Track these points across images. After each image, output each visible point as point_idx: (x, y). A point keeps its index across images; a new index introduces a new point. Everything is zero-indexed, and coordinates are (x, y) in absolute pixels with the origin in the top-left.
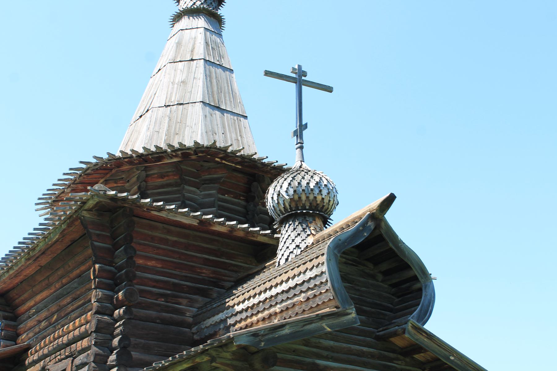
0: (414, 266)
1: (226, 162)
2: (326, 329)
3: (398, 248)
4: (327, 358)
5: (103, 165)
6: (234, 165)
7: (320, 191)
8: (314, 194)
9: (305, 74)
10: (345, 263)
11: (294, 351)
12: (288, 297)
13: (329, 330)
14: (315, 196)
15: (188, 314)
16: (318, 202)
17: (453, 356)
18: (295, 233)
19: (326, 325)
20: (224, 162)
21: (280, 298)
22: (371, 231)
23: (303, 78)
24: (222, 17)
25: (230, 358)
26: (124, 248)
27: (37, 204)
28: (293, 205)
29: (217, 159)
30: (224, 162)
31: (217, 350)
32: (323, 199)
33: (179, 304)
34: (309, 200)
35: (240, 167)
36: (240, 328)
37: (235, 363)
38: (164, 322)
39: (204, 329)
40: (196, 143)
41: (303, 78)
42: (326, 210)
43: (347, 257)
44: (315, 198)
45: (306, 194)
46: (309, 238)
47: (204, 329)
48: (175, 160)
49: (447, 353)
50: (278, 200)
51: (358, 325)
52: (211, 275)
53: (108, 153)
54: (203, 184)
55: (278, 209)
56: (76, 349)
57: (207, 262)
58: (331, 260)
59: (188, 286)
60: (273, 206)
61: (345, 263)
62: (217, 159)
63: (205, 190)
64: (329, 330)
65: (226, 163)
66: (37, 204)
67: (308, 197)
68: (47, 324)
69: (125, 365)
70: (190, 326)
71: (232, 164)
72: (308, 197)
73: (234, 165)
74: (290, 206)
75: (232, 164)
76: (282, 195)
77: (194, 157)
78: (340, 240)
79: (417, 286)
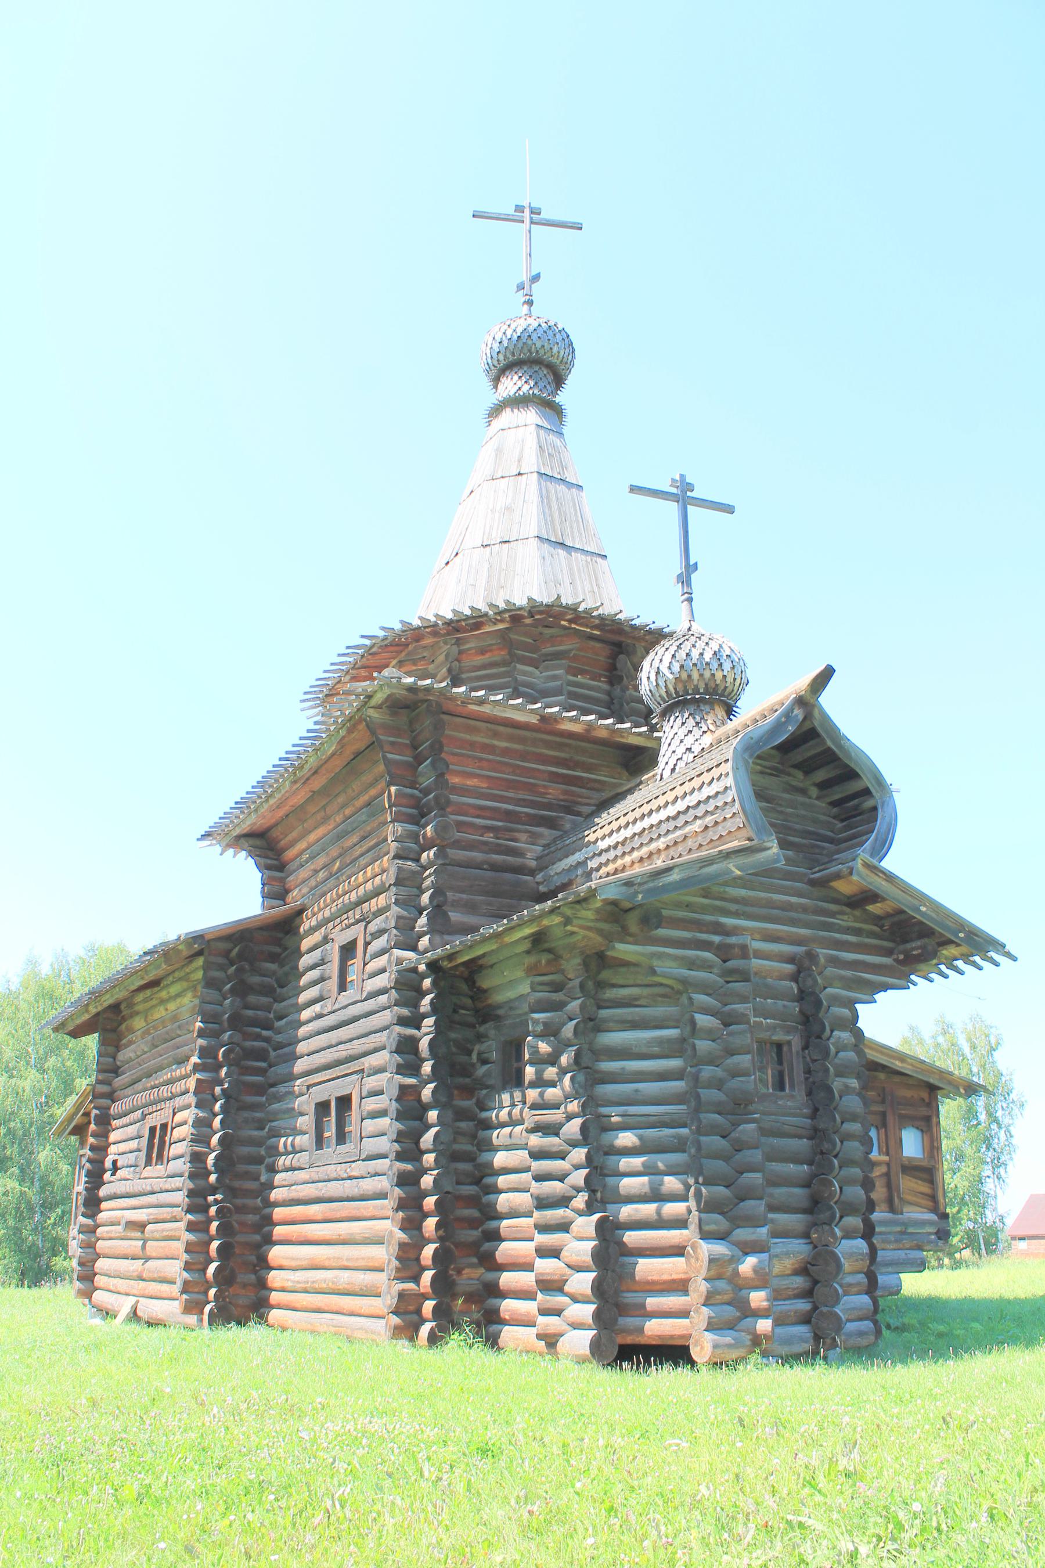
0: (864, 774)
2: (734, 872)
4: (736, 914)
6: (588, 630)
7: (721, 665)
9: (690, 487)
10: (762, 773)
11: (687, 906)
13: (739, 873)
15: (529, 855)
17: (925, 905)
18: (684, 730)
21: (664, 828)
23: (689, 494)
28: (680, 688)
29: (563, 623)
31: (572, 908)
35: (598, 633)
38: (495, 868)
40: (530, 599)
44: (713, 675)
48: (500, 626)
50: (656, 680)
52: (561, 797)
53: (402, 622)
54: (544, 661)
55: (658, 695)
60: (650, 691)
62: (563, 623)
63: (547, 669)
64: (739, 873)
65: (577, 627)
67: (701, 675)
70: (532, 872)
72: (701, 675)
73: (588, 630)
74: (675, 689)
78: (752, 738)
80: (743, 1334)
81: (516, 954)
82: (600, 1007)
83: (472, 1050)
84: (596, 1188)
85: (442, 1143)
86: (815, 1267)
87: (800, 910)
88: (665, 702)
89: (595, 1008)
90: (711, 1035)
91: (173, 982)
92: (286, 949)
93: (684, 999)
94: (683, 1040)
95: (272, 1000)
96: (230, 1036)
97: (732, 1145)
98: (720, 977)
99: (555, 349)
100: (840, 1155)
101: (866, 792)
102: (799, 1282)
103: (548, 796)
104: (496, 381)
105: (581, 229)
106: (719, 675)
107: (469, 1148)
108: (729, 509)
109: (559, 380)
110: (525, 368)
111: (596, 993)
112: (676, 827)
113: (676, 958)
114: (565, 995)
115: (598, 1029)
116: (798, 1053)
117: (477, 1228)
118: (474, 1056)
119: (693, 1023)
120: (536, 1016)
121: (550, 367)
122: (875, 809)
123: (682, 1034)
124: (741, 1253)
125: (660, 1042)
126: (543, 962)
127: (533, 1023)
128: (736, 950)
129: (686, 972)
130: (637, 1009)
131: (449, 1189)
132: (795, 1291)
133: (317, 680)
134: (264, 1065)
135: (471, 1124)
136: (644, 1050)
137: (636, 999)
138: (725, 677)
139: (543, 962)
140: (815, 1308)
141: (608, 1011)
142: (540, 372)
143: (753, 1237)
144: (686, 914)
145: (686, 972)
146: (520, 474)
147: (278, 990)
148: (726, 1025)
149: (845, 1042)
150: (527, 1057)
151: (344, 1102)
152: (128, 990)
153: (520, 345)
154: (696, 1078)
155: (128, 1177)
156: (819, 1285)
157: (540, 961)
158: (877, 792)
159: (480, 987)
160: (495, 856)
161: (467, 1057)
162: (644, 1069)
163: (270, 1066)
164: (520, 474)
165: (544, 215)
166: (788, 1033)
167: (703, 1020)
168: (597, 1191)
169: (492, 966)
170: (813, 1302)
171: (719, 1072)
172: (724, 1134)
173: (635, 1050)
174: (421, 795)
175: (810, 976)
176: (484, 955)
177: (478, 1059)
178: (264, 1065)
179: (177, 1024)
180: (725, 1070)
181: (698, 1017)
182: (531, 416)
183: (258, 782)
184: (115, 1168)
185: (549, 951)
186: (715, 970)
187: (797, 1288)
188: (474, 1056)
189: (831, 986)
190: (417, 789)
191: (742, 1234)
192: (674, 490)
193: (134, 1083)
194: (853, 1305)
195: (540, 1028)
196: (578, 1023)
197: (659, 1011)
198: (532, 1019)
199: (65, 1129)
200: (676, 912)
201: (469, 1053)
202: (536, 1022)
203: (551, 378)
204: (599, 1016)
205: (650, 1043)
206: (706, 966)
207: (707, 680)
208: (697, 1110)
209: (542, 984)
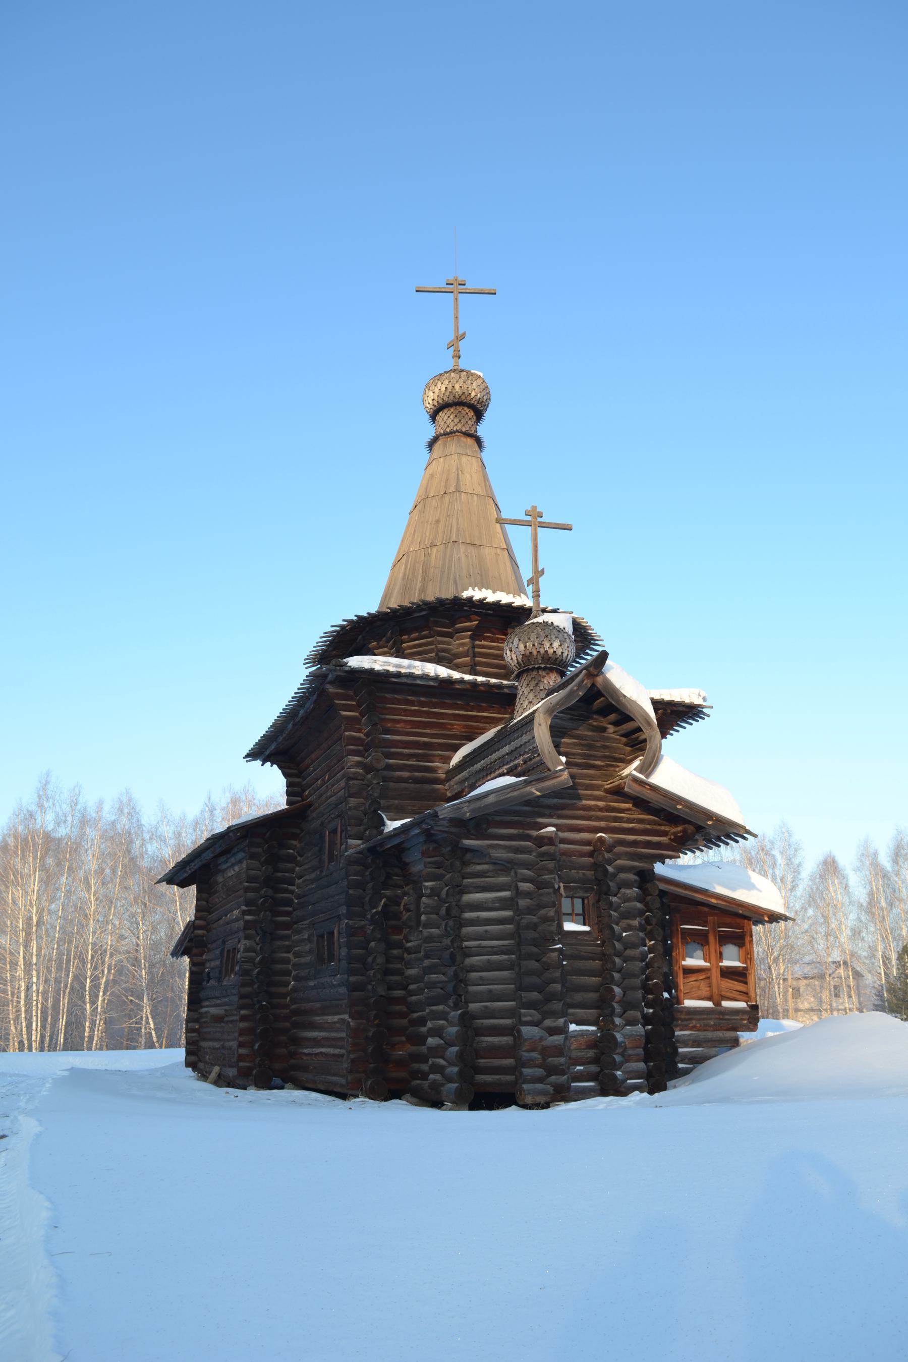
0: (637, 719)
3: (619, 701)
10: (571, 719)
11: (514, 813)
13: (538, 793)
15: (440, 771)
16: (550, 655)
17: (681, 804)
18: (528, 689)
22: (587, 689)
23: (539, 519)
25: (448, 825)
26: (368, 717)
27: (304, 664)
29: (465, 608)
31: (433, 820)
32: (555, 652)
37: (453, 830)
38: (416, 781)
39: (453, 786)
41: (539, 519)
42: (560, 662)
43: (573, 712)
44: (547, 651)
46: (542, 692)
47: (453, 786)
48: (424, 613)
49: (674, 803)
51: (511, 806)
52: (463, 730)
54: (456, 633)
58: (542, 724)
61: (571, 719)
62: (465, 608)
63: (459, 639)
64: (538, 793)
66: (304, 664)
67: (538, 652)
70: (442, 782)
74: (522, 661)
77: (441, 609)
78: (551, 704)
79: (643, 737)
80: (549, 1086)
82: (464, 878)
83: (401, 903)
84: (462, 994)
85: (378, 964)
86: (601, 1044)
88: (519, 669)
89: (460, 879)
90: (528, 895)
91: (238, 852)
92: (303, 831)
93: (512, 873)
94: (511, 899)
95: (294, 865)
96: (265, 891)
97: (542, 966)
99: (473, 394)
100: (622, 971)
101: (639, 730)
102: (591, 1053)
104: (434, 417)
105: (495, 294)
107: (399, 966)
108: (568, 528)
109: (479, 415)
110: (452, 410)
111: (462, 869)
112: (511, 760)
113: (505, 847)
114: (444, 870)
115: (463, 892)
116: (593, 904)
117: (406, 1018)
118: (402, 907)
119: (517, 887)
120: (426, 884)
121: (471, 407)
122: (645, 741)
123: (512, 895)
124: (547, 1035)
125: (500, 899)
126: (431, 848)
127: (425, 888)
128: (58, 975)
129: (511, 855)
131: (383, 993)
132: (589, 1060)
133: (310, 652)
134: (291, 909)
135: (400, 951)
136: (490, 905)
139: (431, 848)
140: (602, 1070)
141: (469, 880)
142: (463, 412)
143: (554, 1024)
144: (513, 818)
145: (511, 855)
147: (299, 858)
148: (539, 889)
149: (629, 896)
150: (422, 910)
151: (331, 934)
152: (422, 671)
153: (447, 394)
154: (518, 924)
156: (604, 1056)
158: (647, 730)
160: (417, 774)
161: (397, 908)
163: (294, 910)
165: (469, 286)
166: (586, 892)
167: (525, 886)
168: (462, 995)
170: (600, 1067)
171: (535, 919)
174: (365, 737)
175: (600, 854)
176: (403, 842)
177: (404, 909)
178: (291, 909)
181: (520, 884)
183: (304, 680)
184: (209, 979)
185: (435, 841)
186: (534, 854)
187: (590, 1057)
188: (402, 907)
189: (620, 859)
190: (362, 733)
191: (548, 1023)
192: (529, 518)
193: (218, 920)
194: (631, 1069)
195: (428, 891)
196: (449, 888)
197: (503, 879)
198: (424, 886)
199: (179, 951)
200: (505, 817)
201: (399, 904)
202: (426, 887)
203: (471, 414)
206: (528, 851)
208: (519, 945)
209: (430, 863)
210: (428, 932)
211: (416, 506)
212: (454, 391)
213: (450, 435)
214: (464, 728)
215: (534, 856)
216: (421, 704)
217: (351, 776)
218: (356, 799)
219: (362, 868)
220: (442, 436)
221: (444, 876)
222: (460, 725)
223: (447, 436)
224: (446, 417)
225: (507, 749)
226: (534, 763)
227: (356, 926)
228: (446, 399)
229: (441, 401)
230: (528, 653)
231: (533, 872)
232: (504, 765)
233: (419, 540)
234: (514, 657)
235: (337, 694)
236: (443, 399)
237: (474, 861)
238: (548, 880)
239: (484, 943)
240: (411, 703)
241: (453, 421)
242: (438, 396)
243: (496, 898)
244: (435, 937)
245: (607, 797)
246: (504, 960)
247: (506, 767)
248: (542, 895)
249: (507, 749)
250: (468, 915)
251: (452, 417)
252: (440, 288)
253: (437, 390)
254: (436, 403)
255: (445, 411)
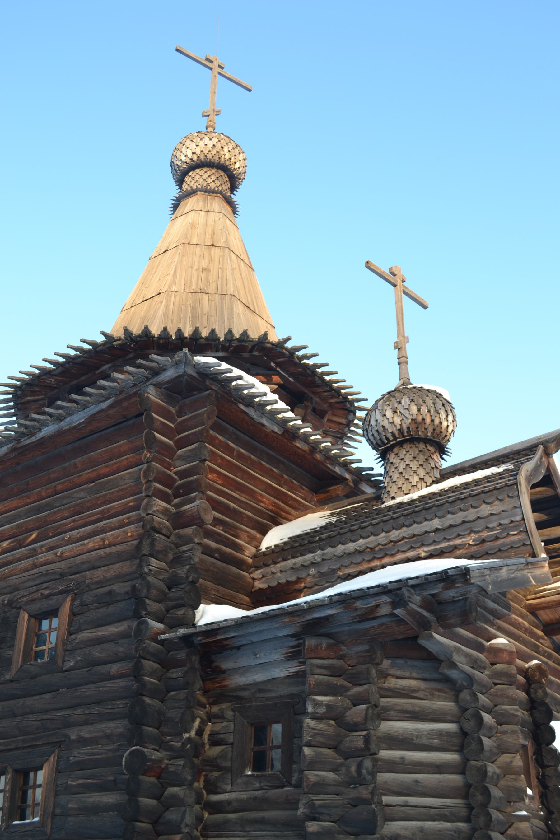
1: (281, 370)
5: (127, 343)
6: (287, 376)
8: (440, 418)
12: (444, 537)
14: (441, 421)
19: (532, 576)
20: (278, 369)
24: (237, 210)
28: (413, 427)
30: (278, 369)
33: (237, 537)
34: (434, 425)
35: (292, 380)
36: (347, 575)
44: (441, 423)
45: (431, 416)
52: (271, 507)
56: (85, 581)
57: (269, 489)
59: (248, 516)
65: (280, 371)
67: (432, 421)
68: (14, 546)
69: (193, 607)
71: (285, 374)
72: (432, 421)
73: (287, 376)
75: (285, 374)
76: (400, 412)
81: (277, 638)
87: (523, 629)
98: (489, 678)
103: (262, 504)
106: (445, 424)
113: (467, 655)
120: (319, 698)
125: (441, 734)
126: (324, 645)
130: (417, 701)
136: (425, 741)
137: (414, 691)
138: (448, 426)
139: (324, 645)
141: (389, 700)
146: (212, 245)
153: (214, 152)
155: (516, 800)
157: (321, 645)
159: (217, 667)
162: (424, 760)
164: (212, 245)
169: (239, 648)
172: (502, 831)
173: (416, 741)
175: (541, 688)
179: (182, 631)
180: (498, 767)
182: (217, 204)
185: (328, 636)
186: (487, 672)
202: (317, 704)
204: (382, 704)
205: (431, 734)
207: (436, 426)
210: (317, 775)
211: (166, 251)
212: (222, 153)
213: (211, 194)
214: (272, 505)
215: (486, 675)
216: (240, 457)
217: (157, 526)
218: (158, 561)
219: (157, 666)
220: (201, 191)
221: (347, 689)
222: (269, 500)
223: (207, 194)
224: (205, 176)
225: (436, 523)
226: (504, 545)
227: (153, 757)
228: (209, 156)
229: (202, 158)
230: (420, 418)
231: (486, 697)
232: (423, 545)
233: (183, 283)
234: (397, 420)
235: (158, 405)
236: (206, 156)
237: (391, 672)
238: (511, 712)
239: (413, 800)
240: (229, 451)
241: (214, 181)
242: (202, 151)
243: (433, 730)
244: (330, 785)
245: (527, 616)
246: (448, 830)
247: (426, 549)
248: (504, 733)
249: (436, 523)
250: (385, 754)
251: (213, 177)
252: (200, 58)
253: (202, 144)
254: (195, 158)
255: (205, 169)
